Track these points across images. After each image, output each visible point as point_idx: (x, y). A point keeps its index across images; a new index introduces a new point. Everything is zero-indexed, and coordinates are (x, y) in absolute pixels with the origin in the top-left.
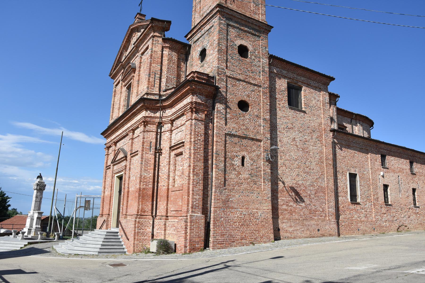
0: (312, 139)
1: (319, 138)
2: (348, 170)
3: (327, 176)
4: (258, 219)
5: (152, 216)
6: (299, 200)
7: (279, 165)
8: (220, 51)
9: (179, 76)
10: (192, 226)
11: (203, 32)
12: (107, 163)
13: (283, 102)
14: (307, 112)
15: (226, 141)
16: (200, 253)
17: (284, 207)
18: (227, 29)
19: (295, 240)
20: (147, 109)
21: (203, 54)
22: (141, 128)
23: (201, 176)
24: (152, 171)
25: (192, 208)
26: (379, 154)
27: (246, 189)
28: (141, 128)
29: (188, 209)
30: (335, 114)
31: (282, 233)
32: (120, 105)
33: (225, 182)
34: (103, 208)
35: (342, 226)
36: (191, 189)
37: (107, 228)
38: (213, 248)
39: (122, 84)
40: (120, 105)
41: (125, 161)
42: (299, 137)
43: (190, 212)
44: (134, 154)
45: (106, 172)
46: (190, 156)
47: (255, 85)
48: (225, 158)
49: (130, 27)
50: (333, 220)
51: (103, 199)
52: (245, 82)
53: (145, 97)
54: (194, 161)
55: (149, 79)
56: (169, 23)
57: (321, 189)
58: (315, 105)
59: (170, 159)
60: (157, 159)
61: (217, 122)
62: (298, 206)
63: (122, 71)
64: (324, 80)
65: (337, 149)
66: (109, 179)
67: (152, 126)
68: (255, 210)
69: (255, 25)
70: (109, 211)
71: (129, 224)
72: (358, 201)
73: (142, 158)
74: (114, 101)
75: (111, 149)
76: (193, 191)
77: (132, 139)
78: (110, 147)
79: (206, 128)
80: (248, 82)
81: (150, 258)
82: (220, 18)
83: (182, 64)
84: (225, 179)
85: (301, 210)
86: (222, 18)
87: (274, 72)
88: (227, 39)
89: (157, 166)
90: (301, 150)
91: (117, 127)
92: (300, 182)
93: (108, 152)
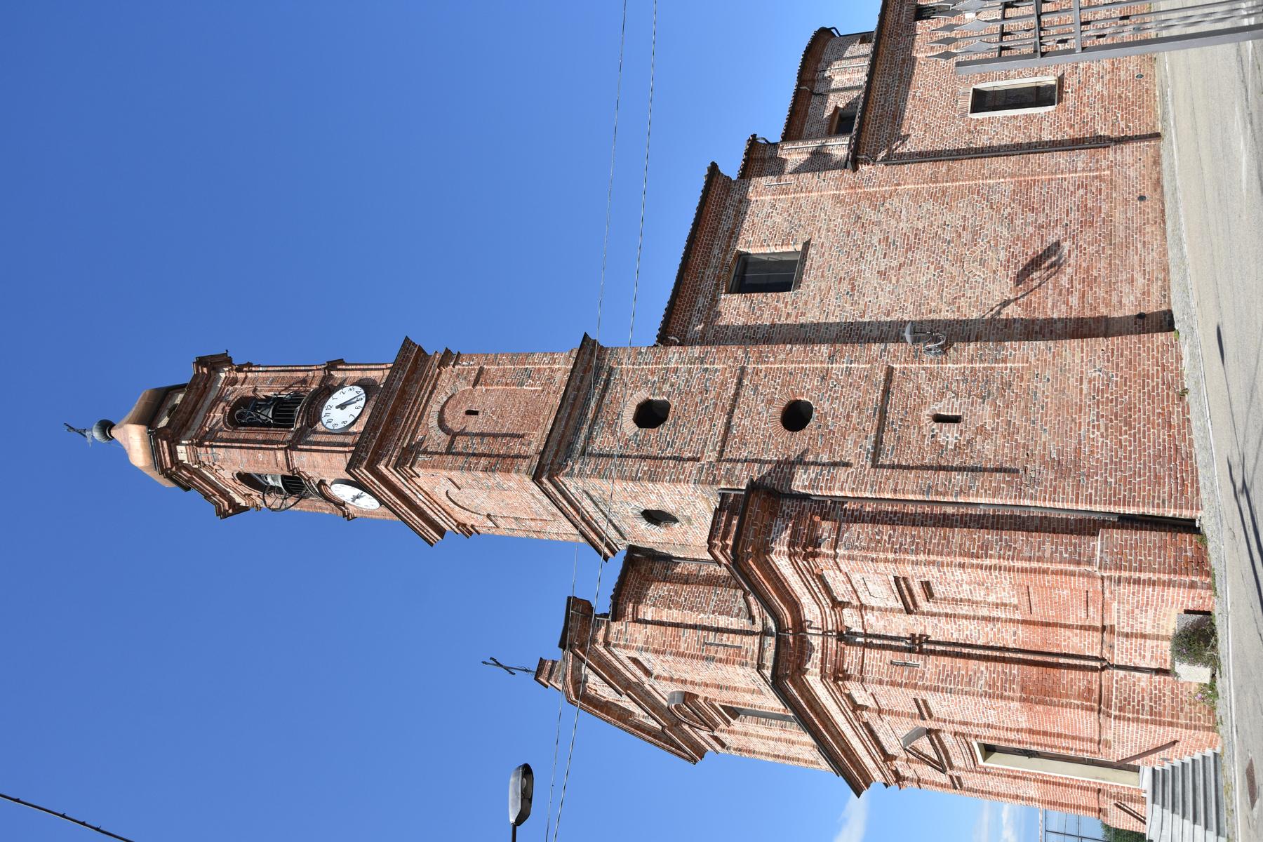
0: (879, 223)
1: (876, 202)
2: (963, 115)
3: (983, 177)
4: (1109, 379)
5: (1103, 669)
6: (1054, 259)
7: (956, 316)
8: (653, 478)
9: (712, 581)
10: (1131, 566)
11: (598, 516)
12: (942, 786)
13: (781, 305)
14: (807, 238)
15: (892, 467)
16: (1210, 546)
17: (1074, 300)
18: (595, 456)
19: (1172, 269)
20: (800, 670)
21: (655, 517)
22: (853, 688)
23: (990, 536)
24: (973, 664)
25: (1079, 563)
26: (915, 26)
27: (1025, 412)
28: (853, 688)
29: (1081, 575)
30: (800, 145)
31: (1151, 307)
32: (780, 740)
33: (1005, 470)
34: (1078, 807)
35: (1127, 126)
36: (1026, 565)
37: (1142, 801)
38: (1198, 509)
39: (722, 731)
40: (780, 740)
41: (942, 735)
42: (874, 262)
43: (1089, 569)
44: (923, 710)
45: (969, 790)
46: (933, 563)
47: (740, 383)
48: (940, 468)
49: (572, 703)
50: (1111, 154)
51: (1049, 803)
52: (732, 411)
53: (768, 673)
54: (948, 554)
55: (721, 661)
56: (572, 602)
57: (1022, 193)
58: (785, 215)
59: (940, 615)
60: (939, 648)
61: (842, 489)
62: (1072, 261)
63: (686, 727)
64: (717, 190)
65: (905, 150)
66: (992, 784)
67: (847, 659)
68: (1085, 386)
69: (581, 381)
70: (1087, 789)
71: (1126, 737)
72: (1053, 83)
73: (936, 689)
74: (768, 755)
75: (907, 773)
76: (1030, 559)
77: (880, 711)
78: (896, 773)
79: (858, 518)
80: (729, 398)
81: (1226, 684)
82: (567, 475)
83: (678, 570)
84: (996, 470)
85: (1083, 251)
86: (568, 469)
87: (703, 331)
88: (621, 456)
89: (957, 650)
90: (910, 254)
91: (843, 751)
92: (1003, 255)
93: (912, 780)
